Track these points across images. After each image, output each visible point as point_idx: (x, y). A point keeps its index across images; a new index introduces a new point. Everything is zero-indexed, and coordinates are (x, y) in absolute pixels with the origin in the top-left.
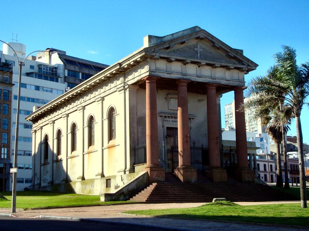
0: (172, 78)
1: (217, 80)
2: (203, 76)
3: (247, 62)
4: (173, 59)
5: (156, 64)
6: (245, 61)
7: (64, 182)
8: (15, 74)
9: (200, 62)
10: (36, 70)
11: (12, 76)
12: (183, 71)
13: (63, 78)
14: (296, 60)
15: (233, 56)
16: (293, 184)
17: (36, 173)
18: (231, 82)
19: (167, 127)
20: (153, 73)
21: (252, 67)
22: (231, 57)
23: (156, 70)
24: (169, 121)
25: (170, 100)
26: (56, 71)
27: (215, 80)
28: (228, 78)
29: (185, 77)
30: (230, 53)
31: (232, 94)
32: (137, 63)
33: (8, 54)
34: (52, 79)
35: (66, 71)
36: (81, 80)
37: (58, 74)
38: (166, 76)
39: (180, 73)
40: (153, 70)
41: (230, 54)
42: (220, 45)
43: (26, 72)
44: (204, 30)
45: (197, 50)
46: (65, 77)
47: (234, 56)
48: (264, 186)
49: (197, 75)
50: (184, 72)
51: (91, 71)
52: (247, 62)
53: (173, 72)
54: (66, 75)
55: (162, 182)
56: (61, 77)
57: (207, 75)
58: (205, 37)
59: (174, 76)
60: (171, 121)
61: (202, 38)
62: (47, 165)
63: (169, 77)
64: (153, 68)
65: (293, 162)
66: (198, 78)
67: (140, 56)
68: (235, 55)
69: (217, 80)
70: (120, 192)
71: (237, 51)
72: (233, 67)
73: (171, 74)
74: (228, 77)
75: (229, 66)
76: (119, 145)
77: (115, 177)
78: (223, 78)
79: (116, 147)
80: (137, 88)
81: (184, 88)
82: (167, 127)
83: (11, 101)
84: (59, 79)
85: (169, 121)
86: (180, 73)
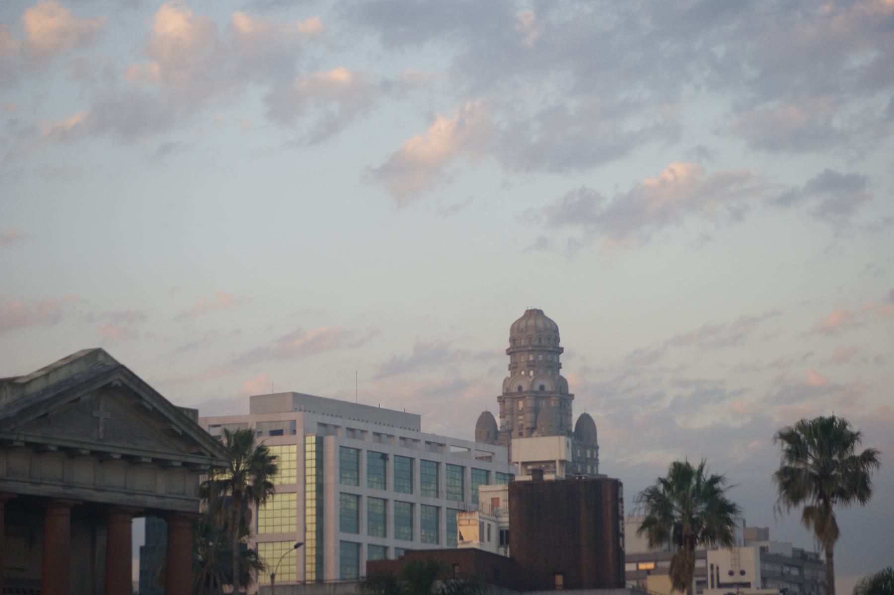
0: (41, 494)
1: (138, 497)
3: (210, 449)
6: (206, 446)
8: (281, 448)
9: (109, 453)
14: (807, 524)
15: (180, 432)
18: (167, 500)
21: (221, 461)
27: (132, 498)
28: (231, 476)
30: (176, 425)
38: (29, 489)
41: (174, 428)
42: (155, 405)
44: (123, 367)
47: (183, 432)
52: (210, 449)
55: (524, 346)
58: (124, 384)
59: (44, 490)
61: (116, 387)
63: (35, 493)
68: (186, 430)
69: (138, 497)
71: (185, 413)
72: (179, 464)
74: (161, 489)
75: (171, 461)
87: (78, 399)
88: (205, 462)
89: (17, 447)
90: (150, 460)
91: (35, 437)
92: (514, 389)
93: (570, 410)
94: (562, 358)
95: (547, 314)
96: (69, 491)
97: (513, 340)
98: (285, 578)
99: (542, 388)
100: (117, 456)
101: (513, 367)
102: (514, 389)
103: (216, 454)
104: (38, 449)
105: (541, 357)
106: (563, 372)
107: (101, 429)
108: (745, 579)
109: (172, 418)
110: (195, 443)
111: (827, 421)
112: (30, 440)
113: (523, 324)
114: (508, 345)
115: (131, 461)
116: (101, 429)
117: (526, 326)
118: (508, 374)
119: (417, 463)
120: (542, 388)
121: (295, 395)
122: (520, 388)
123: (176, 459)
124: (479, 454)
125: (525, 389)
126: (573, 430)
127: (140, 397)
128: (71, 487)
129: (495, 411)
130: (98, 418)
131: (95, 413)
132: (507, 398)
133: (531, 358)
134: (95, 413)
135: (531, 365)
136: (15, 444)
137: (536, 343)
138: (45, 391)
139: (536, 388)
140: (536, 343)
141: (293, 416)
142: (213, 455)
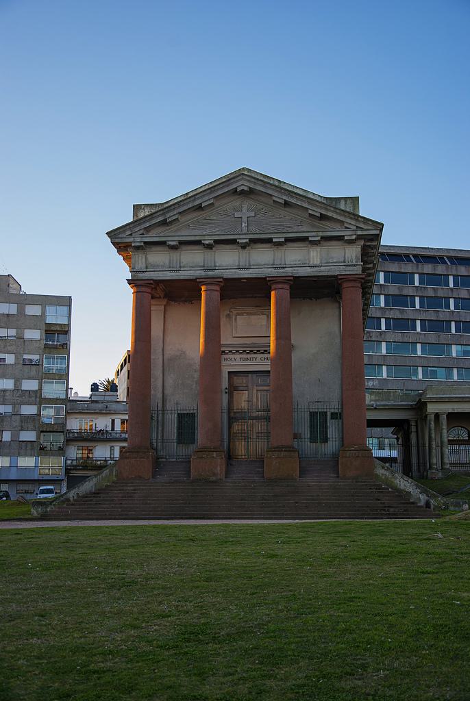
2: (253, 265)
5: (148, 256)
12: (206, 262)
16: (17, 381)
20: (140, 275)
23: (147, 267)
24: (233, 360)
25: (236, 319)
29: (210, 273)
38: (169, 276)
39: (200, 267)
40: (211, 266)
42: (284, 198)
45: (240, 216)
49: (344, 262)
50: (210, 264)
51: (403, 265)
53: (184, 267)
57: (263, 263)
59: (184, 275)
60: (238, 359)
64: (315, 254)
65: (460, 397)
66: (242, 272)
78: (269, 265)
80: (165, 303)
82: (229, 372)
85: (233, 360)
86: (200, 267)
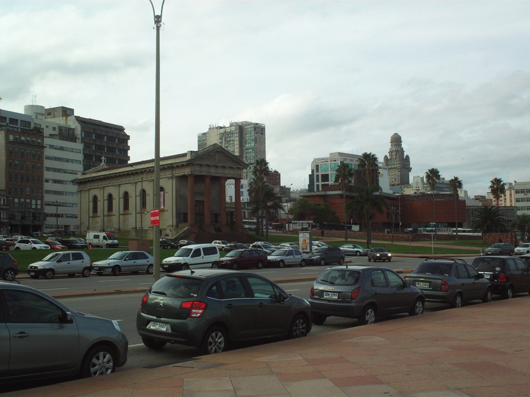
1: (226, 175)
4: (204, 165)
7: (117, 231)
10: (57, 132)
11: (44, 139)
13: (80, 139)
16: (513, 236)
17: (82, 222)
19: (196, 201)
22: (234, 161)
26: (73, 132)
31: (233, 181)
32: (183, 166)
33: (25, 112)
34: (72, 141)
35: (83, 133)
36: (94, 140)
37: (75, 135)
38: (200, 174)
43: (49, 134)
46: (82, 138)
48: (232, 241)
54: (83, 136)
56: (79, 138)
58: (221, 151)
59: (203, 174)
61: (219, 151)
62: (96, 218)
67: (186, 163)
70: (72, 241)
71: (237, 157)
72: (228, 167)
73: (202, 172)
74: (232, 173)
76: (168, 211)
77: (165, 229)
79: (166, 212)
81: (208, 181)
83: (43, 161)
84: (77, 140)
87: (210, 154)
88: (242, 167)
89: (195, 165)
90: (228, 167)
91: (199, 162)
92: (392, 150)
93: (404, 154)
94: (402, 143)
95: (398, 134)
96: (209, 174)
97: (391, 140)
98: (279, 190)
99: (398, 150)
100: (220, 166)
101: (392, 145)
102: (392, 150)
103: (245, 165)
104: (201, 165)
105: (397, 143)
106: (402, 146)
107: (217, 160)
108: (419, 189)
109: (233, 158)
110: (239, 163)
111: (368, 154)
112: (198, 163)
113: (393, 136)
114: (390, 141)
115: (224, 167)
116: (217, 160)
117: (394, 137)
118: (390, 147)
119: (353, 164)
120: (398, 150)
121: (339, 153)
122: (393, 150)
123: (235, 167)
124: (328, 165)
125: (394, 150)
126: (405, 158)
127: (225, 154)
128: (210, 173)
129: (388, 155)
130: (216, 158)
131: (215, 157)
132: (391, 152)
133: (395, 143)
134: (215, 157)
135: (395, 145)
136: (195, 164)
137: (396, 140)
138: (203, 153)
139: (396, 150)
140: (396, 140)
141: (338, 157)
142: (244, 166)
